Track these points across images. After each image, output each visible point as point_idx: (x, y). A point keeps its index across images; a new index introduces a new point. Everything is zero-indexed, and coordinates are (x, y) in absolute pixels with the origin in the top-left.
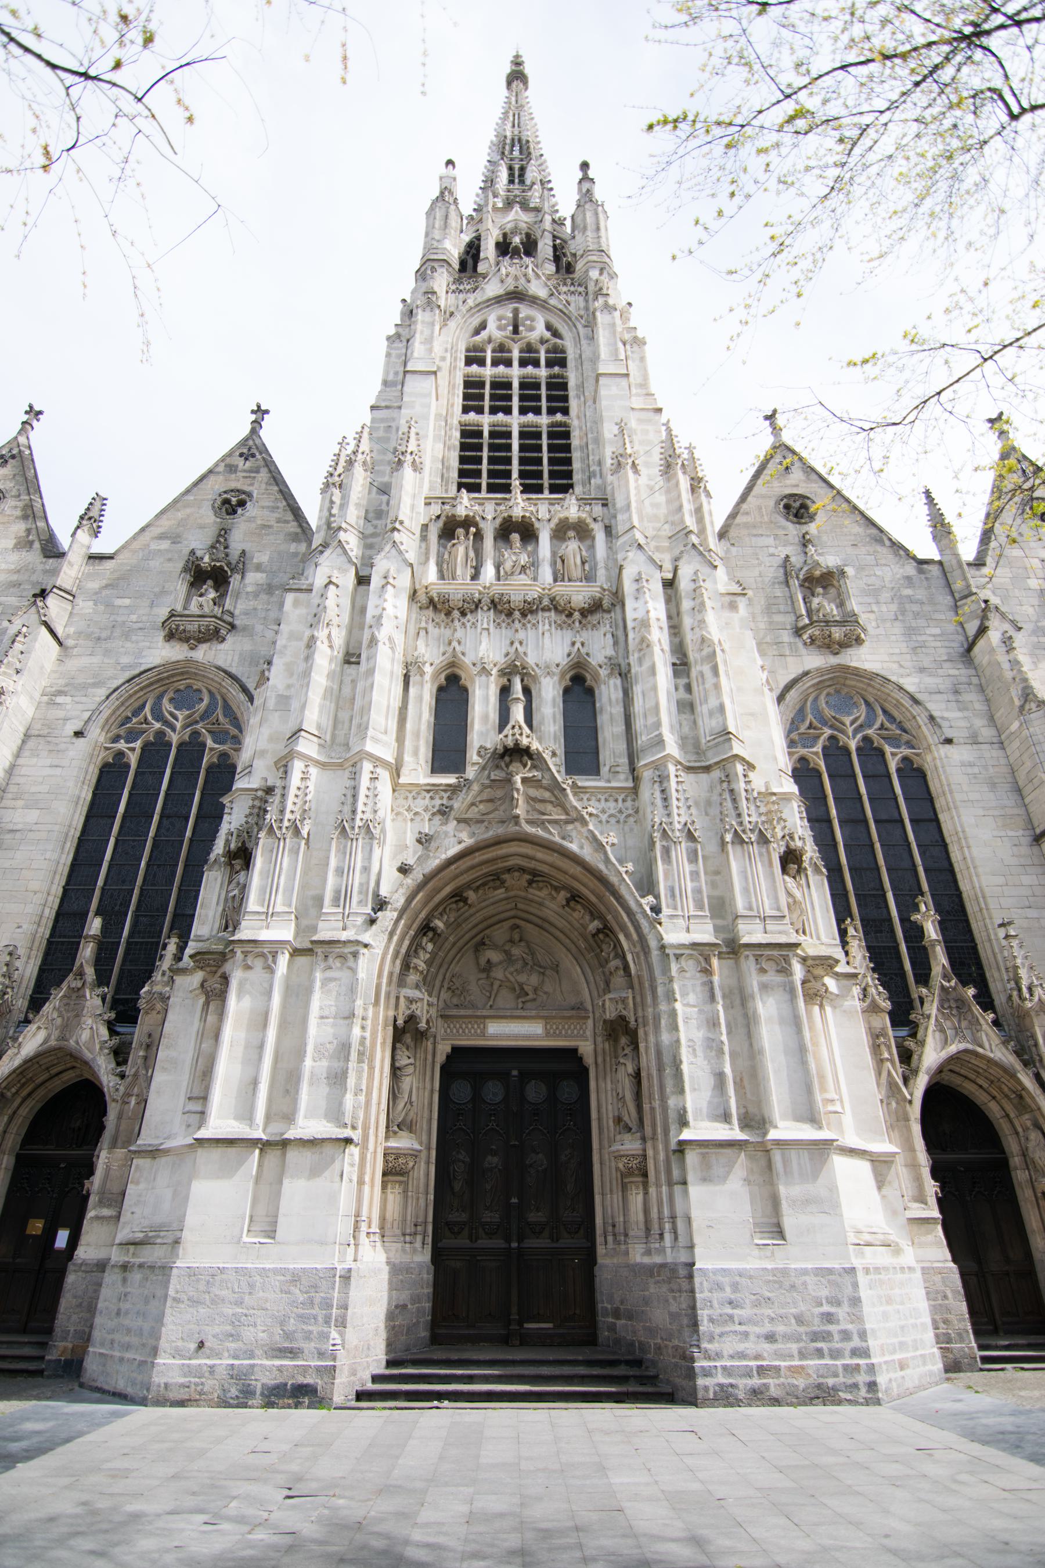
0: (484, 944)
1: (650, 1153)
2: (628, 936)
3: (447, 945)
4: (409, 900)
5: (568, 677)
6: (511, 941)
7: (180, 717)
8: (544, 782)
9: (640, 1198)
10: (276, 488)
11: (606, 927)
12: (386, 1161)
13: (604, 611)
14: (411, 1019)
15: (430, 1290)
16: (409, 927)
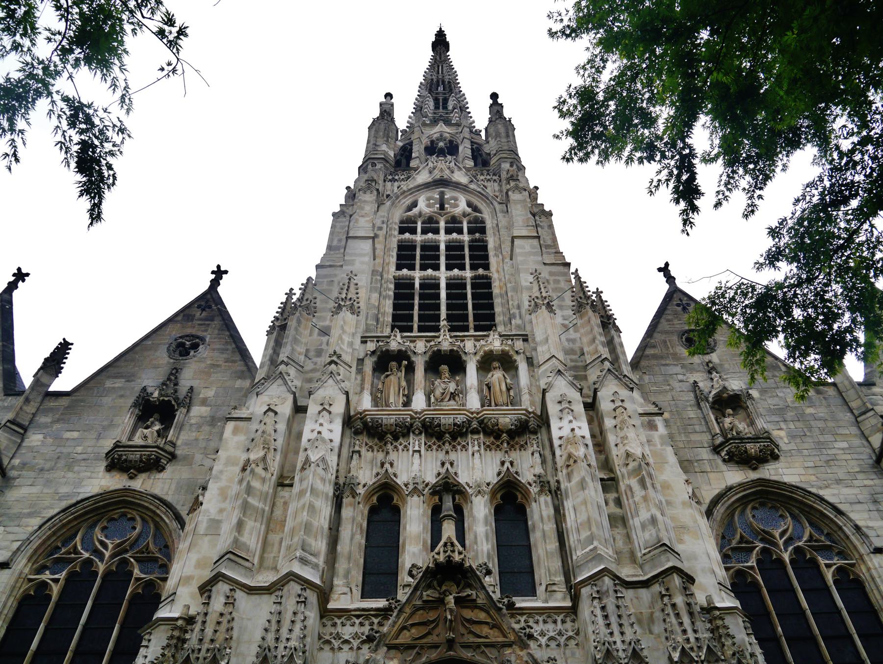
5: (499, 496)
7: (110, 546)
10: (227, 333)
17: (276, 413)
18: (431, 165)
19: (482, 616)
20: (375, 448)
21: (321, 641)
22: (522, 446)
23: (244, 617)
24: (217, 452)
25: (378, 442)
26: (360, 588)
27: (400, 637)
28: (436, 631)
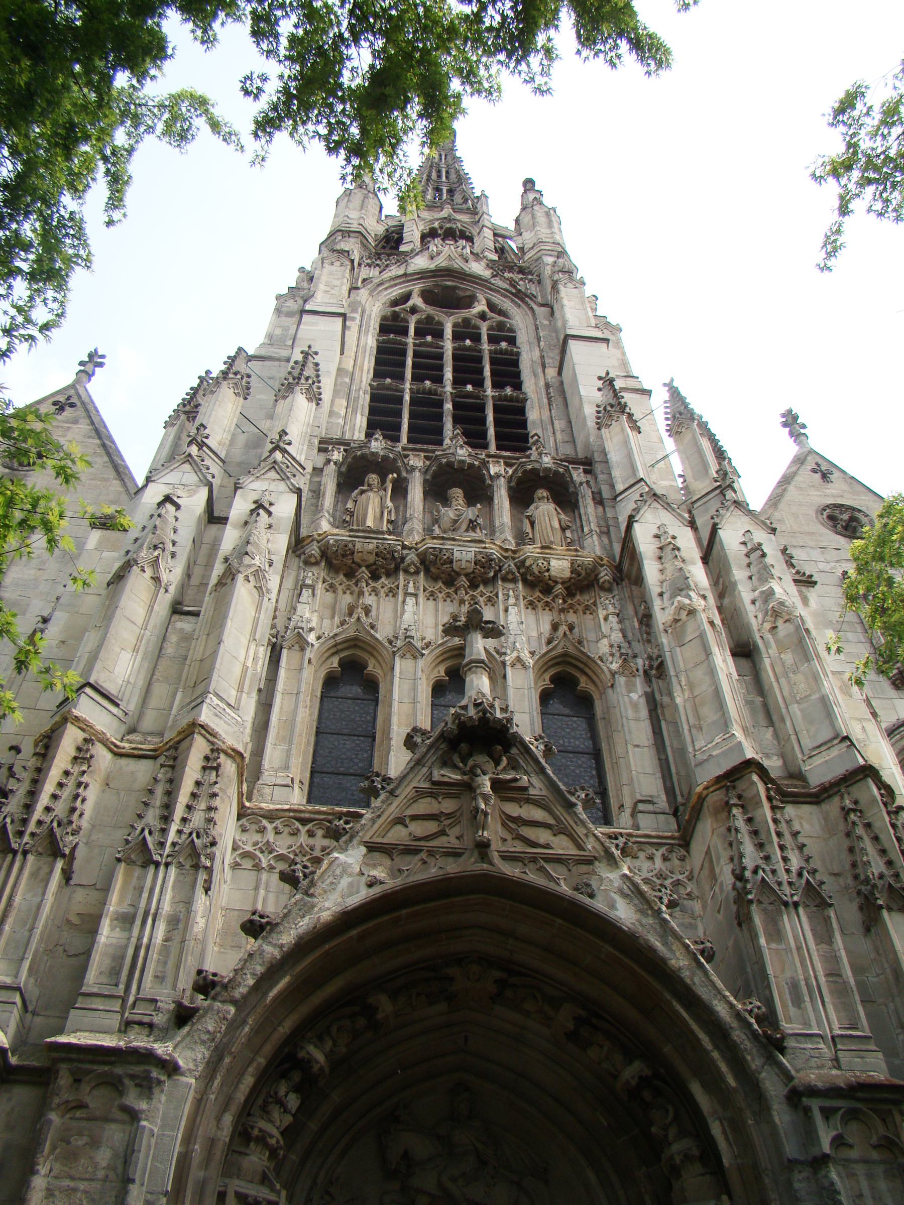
2: (714, 1084)
5: (547, 676)
8: (532, 791)
10: (98, 441)
13: (602, 588)
17: (178, 507)
18: (433, 248)
19: (538, 814)
20: (340, 589)
21: (238, 852)
22: (587, 608)
25: (344, 580)
26: (306, 788)
27: (390, 835)
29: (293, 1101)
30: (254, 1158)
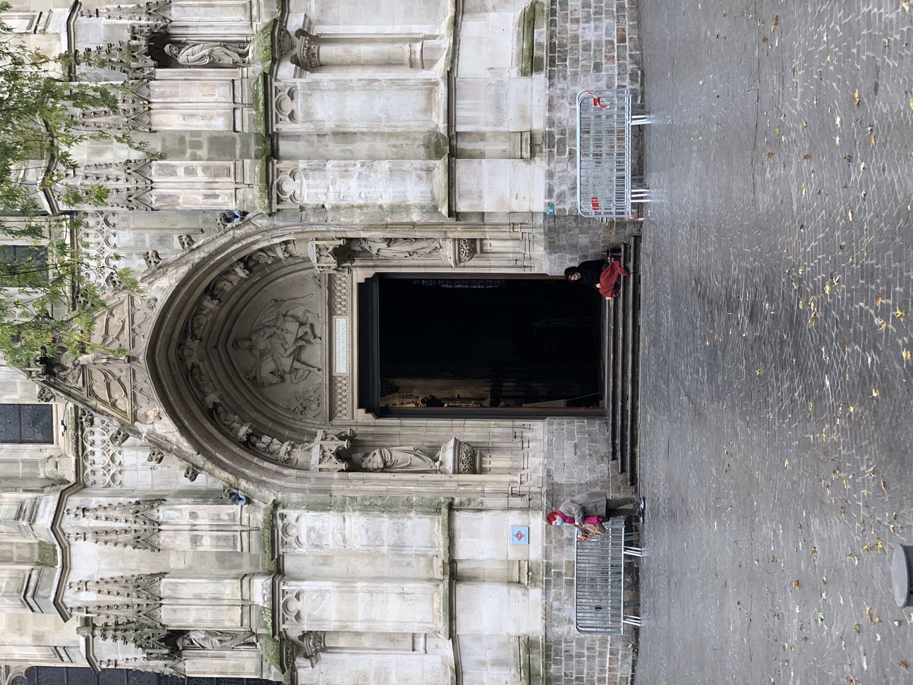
0: (255, 378)
1: (457, 235)
2: (254, 243)
3: (261, 419)
4: (224, 467)
6: (251, 348)
9: (494, 243)
11: (241, 260)
12: (464, 472)
14: (340, 455)
15: (565, 421)
16: (249, 464)
19: (99, 325)
23: (97, 569)
24: (80, 608)
28: (117, 373)
29: (266, 439)
30: (299, 456)
